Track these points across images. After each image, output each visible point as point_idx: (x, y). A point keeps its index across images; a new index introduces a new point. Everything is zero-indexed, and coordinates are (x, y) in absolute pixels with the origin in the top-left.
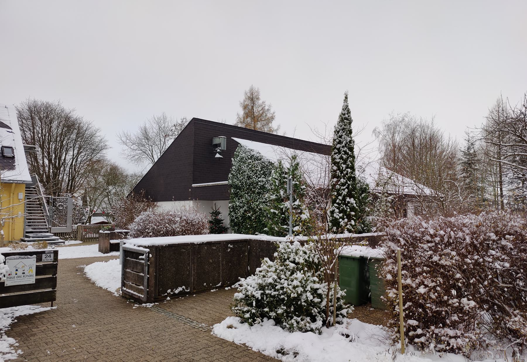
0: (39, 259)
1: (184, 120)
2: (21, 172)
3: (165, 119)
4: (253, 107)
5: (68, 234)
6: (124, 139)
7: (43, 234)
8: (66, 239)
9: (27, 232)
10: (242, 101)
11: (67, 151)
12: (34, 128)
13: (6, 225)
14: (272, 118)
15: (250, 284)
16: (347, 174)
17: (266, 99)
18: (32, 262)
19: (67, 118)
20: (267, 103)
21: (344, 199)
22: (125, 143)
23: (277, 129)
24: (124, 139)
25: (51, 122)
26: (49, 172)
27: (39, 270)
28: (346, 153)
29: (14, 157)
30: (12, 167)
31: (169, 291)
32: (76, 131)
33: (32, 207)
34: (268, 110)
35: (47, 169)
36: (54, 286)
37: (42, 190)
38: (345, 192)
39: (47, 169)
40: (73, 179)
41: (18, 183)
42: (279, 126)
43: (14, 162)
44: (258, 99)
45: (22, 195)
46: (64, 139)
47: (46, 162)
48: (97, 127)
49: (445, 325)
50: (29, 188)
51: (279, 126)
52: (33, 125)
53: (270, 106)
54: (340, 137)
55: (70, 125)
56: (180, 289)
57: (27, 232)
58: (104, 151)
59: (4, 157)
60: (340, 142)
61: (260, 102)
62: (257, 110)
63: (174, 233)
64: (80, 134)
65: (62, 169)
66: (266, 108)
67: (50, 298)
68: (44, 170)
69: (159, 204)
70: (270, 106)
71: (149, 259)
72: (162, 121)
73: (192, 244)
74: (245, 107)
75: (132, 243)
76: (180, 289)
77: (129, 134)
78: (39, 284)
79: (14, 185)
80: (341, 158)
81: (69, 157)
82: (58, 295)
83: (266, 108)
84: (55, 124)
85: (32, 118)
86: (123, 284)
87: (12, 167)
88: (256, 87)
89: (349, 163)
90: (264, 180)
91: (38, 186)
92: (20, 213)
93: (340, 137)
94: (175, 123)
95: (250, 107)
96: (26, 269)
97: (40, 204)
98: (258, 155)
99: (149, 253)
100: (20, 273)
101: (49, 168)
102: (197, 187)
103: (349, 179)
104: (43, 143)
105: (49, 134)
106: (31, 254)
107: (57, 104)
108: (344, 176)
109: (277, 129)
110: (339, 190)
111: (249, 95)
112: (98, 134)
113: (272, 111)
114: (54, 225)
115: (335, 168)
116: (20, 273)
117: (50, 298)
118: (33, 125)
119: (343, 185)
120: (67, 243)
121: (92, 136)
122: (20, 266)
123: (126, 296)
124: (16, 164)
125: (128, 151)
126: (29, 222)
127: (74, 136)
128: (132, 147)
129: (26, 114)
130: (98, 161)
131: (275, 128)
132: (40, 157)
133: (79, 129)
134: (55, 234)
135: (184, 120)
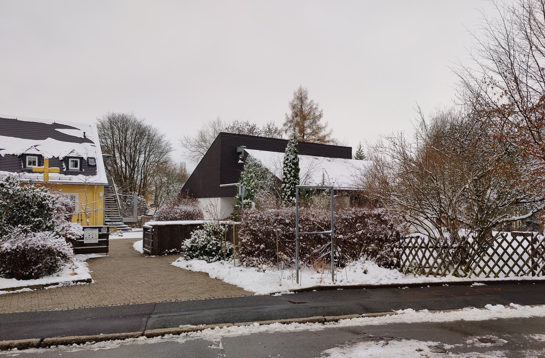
0: (100, 231)
1: (236, 123)
2: (101, 177)
3: (219, 123)
4: (301, 106)
5: (133, 223)
6: (185, 142)
7: (117, 223)
8: (133, 227)
9: (106, 222)
10: (291, 101)
11: (140, 154)
12: (113, 137)
13: (92, 215)
14: (320, 116)
15: (187, 243)
16: (290, 181)
17: (312, 98)
18: (96, 232)
19: (139, 126)
20: (315, 102)
21: (289, 198)
22: (185, 146)
23: (325, 127)
24: (185, 142)
25: (127, 130)
26: (126, 173)
27: (100, 236)
28: (290, 167)
29: (96, 165)
30: (94, 173)
31: (167, 250)
32: (146, 137)
33: (109, 202)
34: (316, 108)
35: (124, 170)
36: (108, 245)
37: (116, 189)
38: (289, 193)
39: (124, 170)
40: (145, 177)
41: (99, 185)
42: (327, 123)
43: (96, 169)
44: (306, 98)
45: (102, 194)
46: (137, 145)
47: (123, 164)
48: (162, 134)
49: (253, 256)
50: (107, 189)
51: (327, 123)
52: (113, 133)
53: (317, 105)
54: (288, 156)
55: (142, 132)
56: (173, 250)
57: (106, 222)
58: (170, 153)
59: (89, 165)
60: (287, 159)
61: (308, 101)
62: (306, 109)
63: (176, 219)
64: (150, 139)
65: (136, 169)
66: (314, 106)
67: (106, 251)
68: (122, 171)
69: (199, 200)
70: (317, 105)
71: (152, 232)
72: (217, 125)
73: (181, 225)
74: (294, 107)
75: (147, 224)
76: (173, 250)
77: (189, 137)
78: (100, 243)
79: (96, 186)
80: (288, 170)
81: (142, 158)
82: (109, 249)
83: (314, 106)
84: (129, 133)
85: (112, 128)
86: (144, 247)
87: (94, 173)
88: (304, 87)
89: (292, 173)
90: (263, 182)
91: (114, 187)
92: (101, 207)
93: (288, 156)
94: (227, 127)
95: (299, 107)
96: (94, 235)
97: (115, 200)
98: (259, 163)
99: (152, 228)
100: (91, 237)
101: (126, 168)
102: (223, 187)
103: (292, 184)
104: (121, 148)
105: (125, 141)
106: (96, 228)
107: (130, 115)
108: (289, 182)
109: (325, 127)
110: (286, 192)
111: (297, 94)
112: (163, 139)
113: (319, 110)
114: (125, 216)
115: (284, 177)
116: (91, 237)
117: (106, 251)
118: (113, 133)
119: (288, 188)
120: (133, 230)
121: (159, 141)
122: (91, 234)
123: (146, 253)
124: (97, 171)
125: (188, 153)
126: (107, 213)
127: (144, 141)
128: (191, 149)
129: (107, 125)
130: (166, 162)
131: (324, 126)
132: (118, 161)
133: (149, 136)
134: (125, 223)
135: (236, 123)
